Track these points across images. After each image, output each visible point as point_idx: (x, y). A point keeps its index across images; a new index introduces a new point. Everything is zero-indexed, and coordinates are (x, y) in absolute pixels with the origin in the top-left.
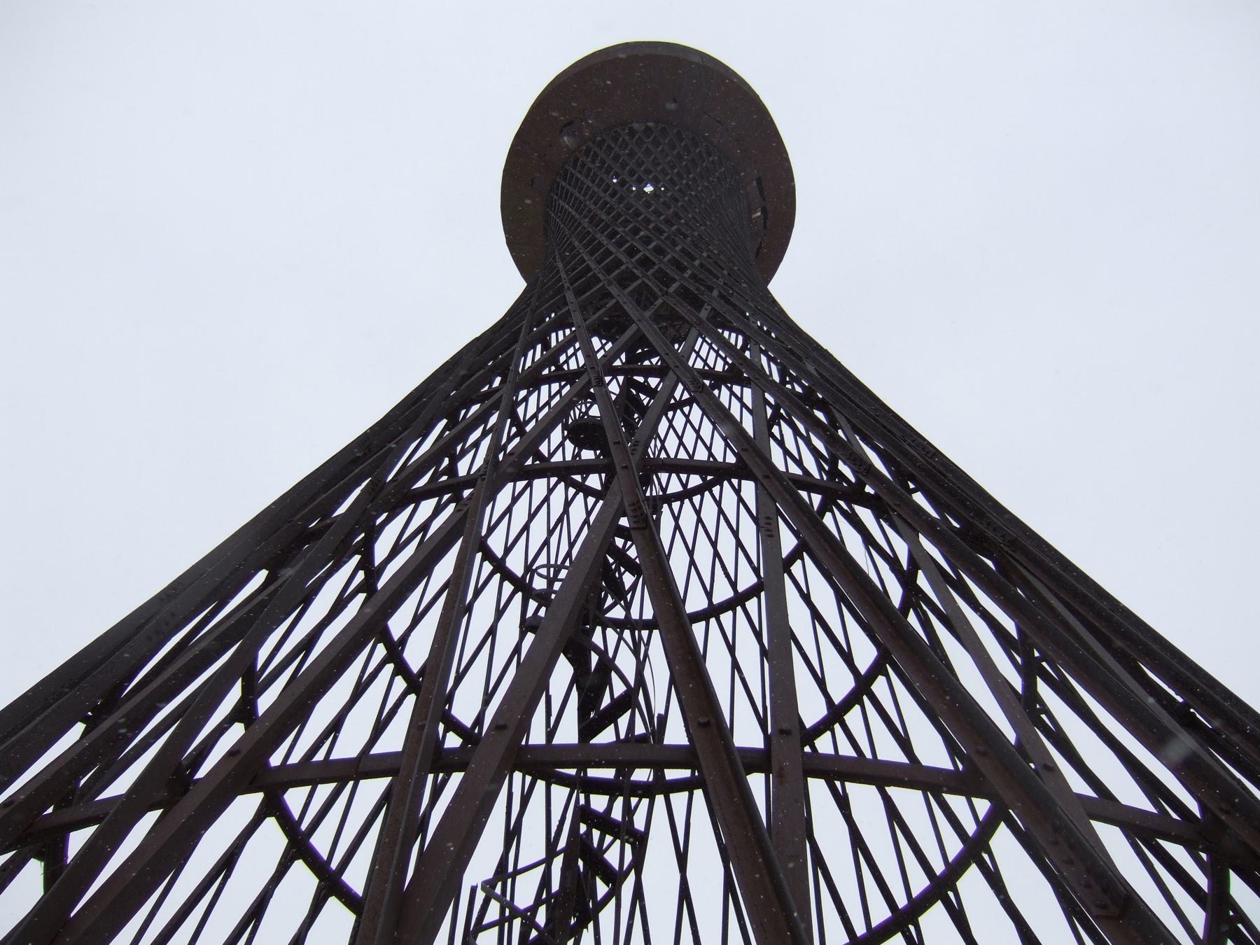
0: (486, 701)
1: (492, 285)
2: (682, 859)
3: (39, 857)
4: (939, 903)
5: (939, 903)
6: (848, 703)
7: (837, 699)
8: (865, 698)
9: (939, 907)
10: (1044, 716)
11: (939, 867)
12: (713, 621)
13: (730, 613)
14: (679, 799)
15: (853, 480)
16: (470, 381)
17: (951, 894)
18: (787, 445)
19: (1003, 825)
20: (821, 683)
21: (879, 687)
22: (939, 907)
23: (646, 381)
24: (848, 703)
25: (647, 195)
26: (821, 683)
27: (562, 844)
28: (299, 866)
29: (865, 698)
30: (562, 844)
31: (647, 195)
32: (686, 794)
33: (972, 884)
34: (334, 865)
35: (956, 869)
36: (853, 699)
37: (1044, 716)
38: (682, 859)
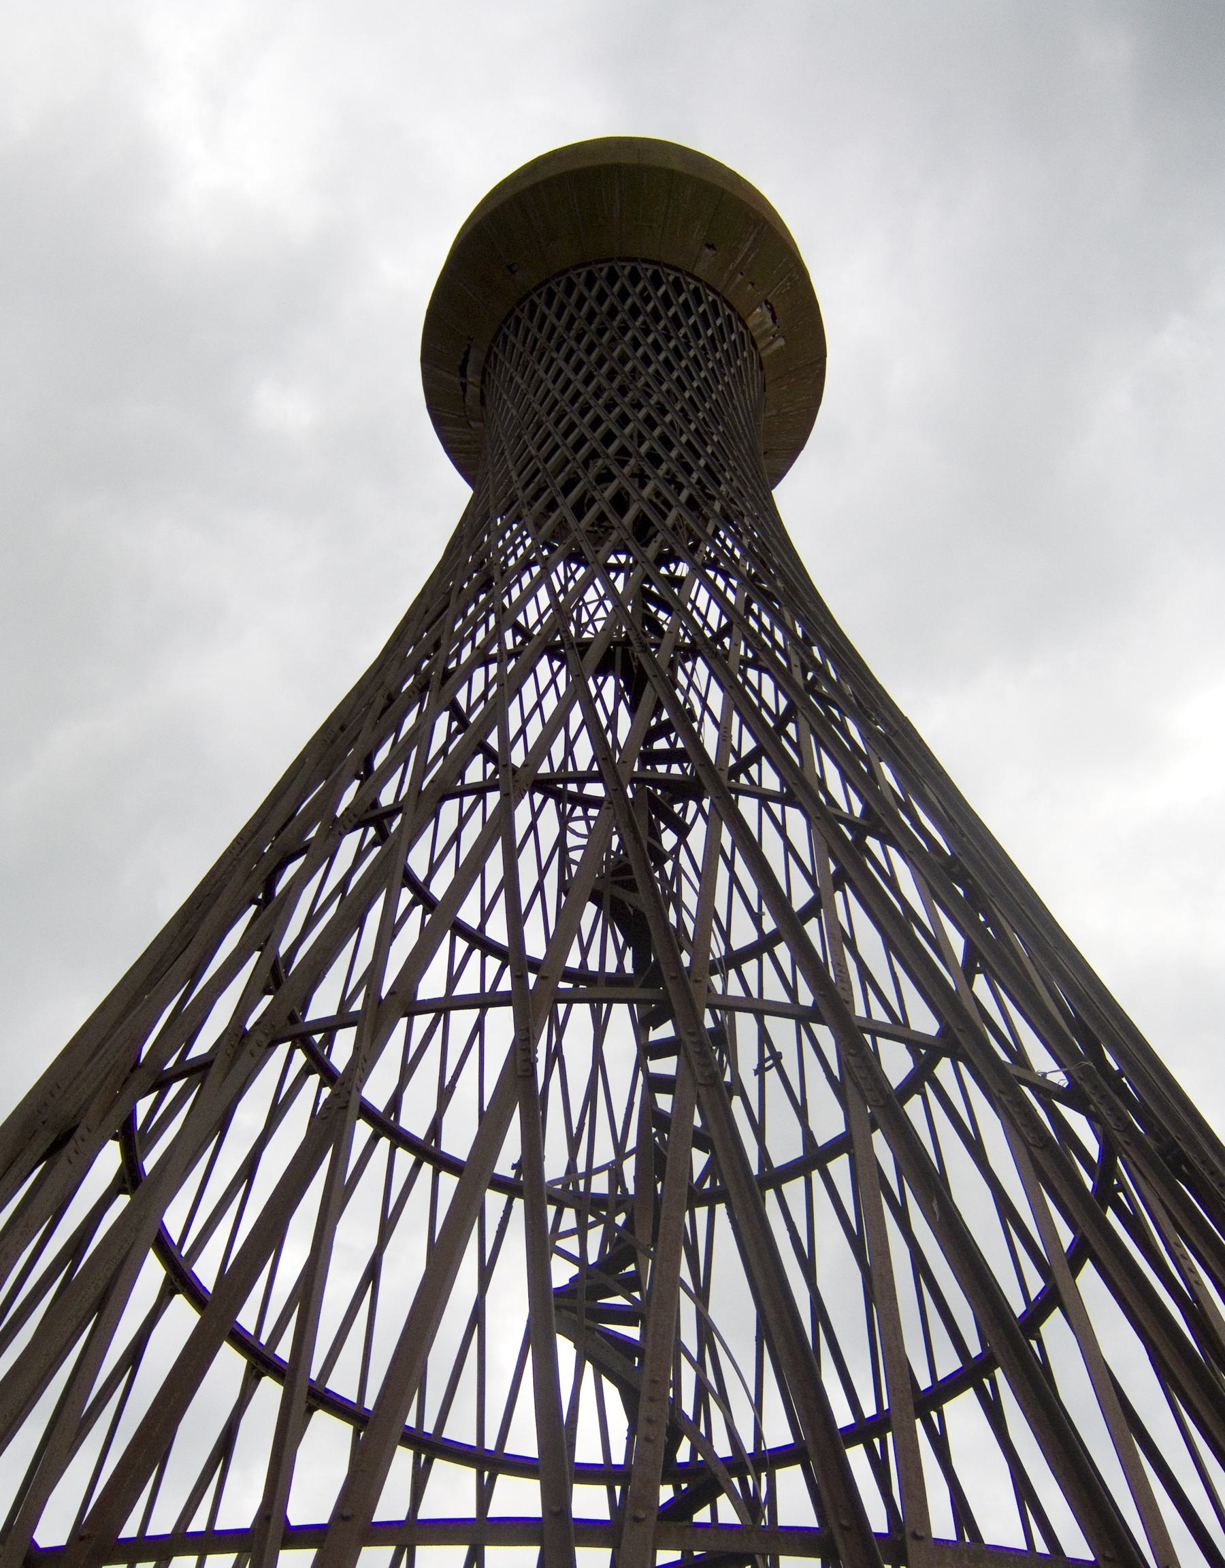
1: (436, 497)
3: (115, 1138)
4: (971, 1391)
5: (971, 1391)
9: (969, 1395)
10: (1121, 1195)
13: (754, 962)
15: (631, 1191)
16: (466, 576)
17: (986, 1382)
18: (727, 874)
21: (944, 1070)
22: (969, 1395)
23: (656, 612)
25: (617, 338)
27: (632, 1143)
30: (632, 1143)
31: (617, 338)
32: (508, 1449)
34: (264, 1339)
37: (1121, 1195)
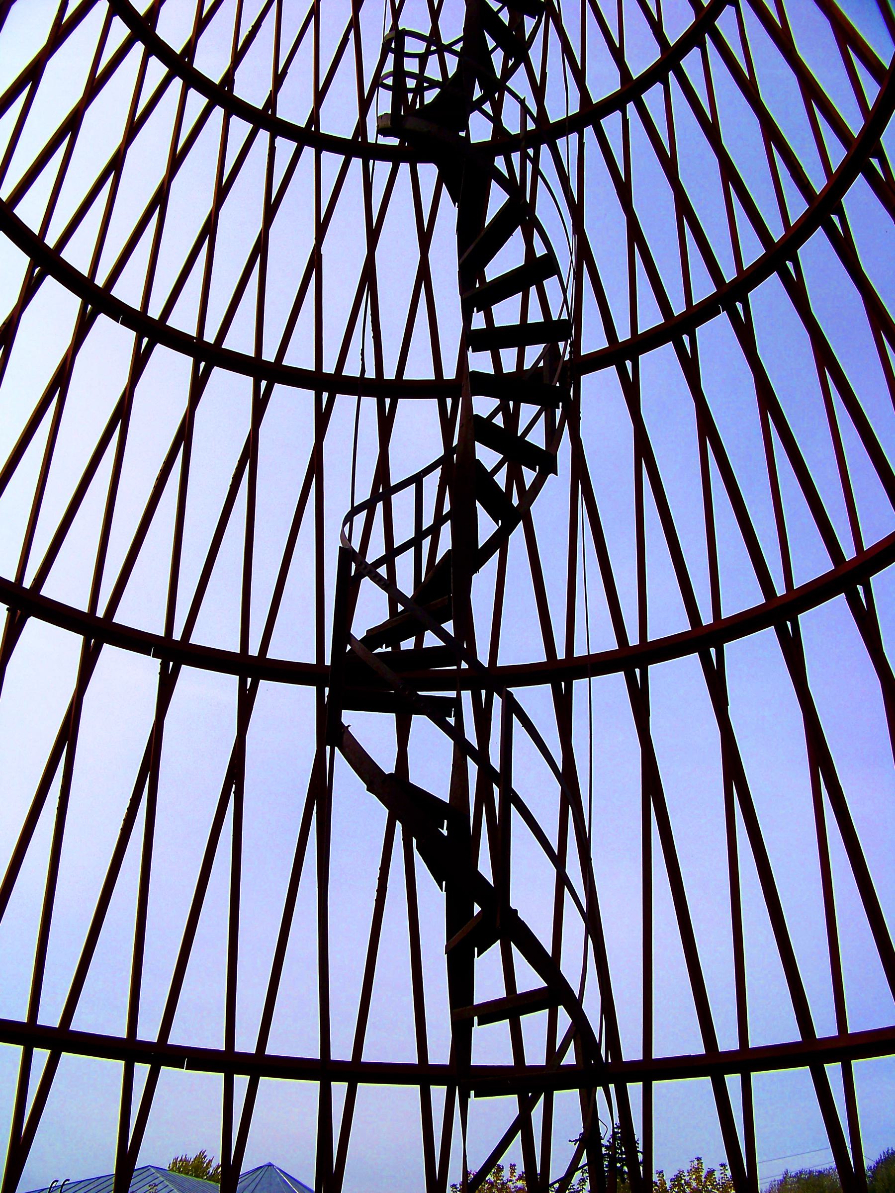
0: (565, 291)
2: (271, 210)
6: (647, 80)
7: (636, 71)
8: (671, 74)
9: (723, 318)
11: (729, 274)
12: (589, 131)
14: (382, 169)
19: (546, 1011)
20: (618, 54)
22: (723, 318)
24: (647, 80)
26: (618, 54)
28: (51, 285)
29: (671, 74)
33: (768, 299)
35: (750, 278)
36: (656, 75)
38: (271, 210)
